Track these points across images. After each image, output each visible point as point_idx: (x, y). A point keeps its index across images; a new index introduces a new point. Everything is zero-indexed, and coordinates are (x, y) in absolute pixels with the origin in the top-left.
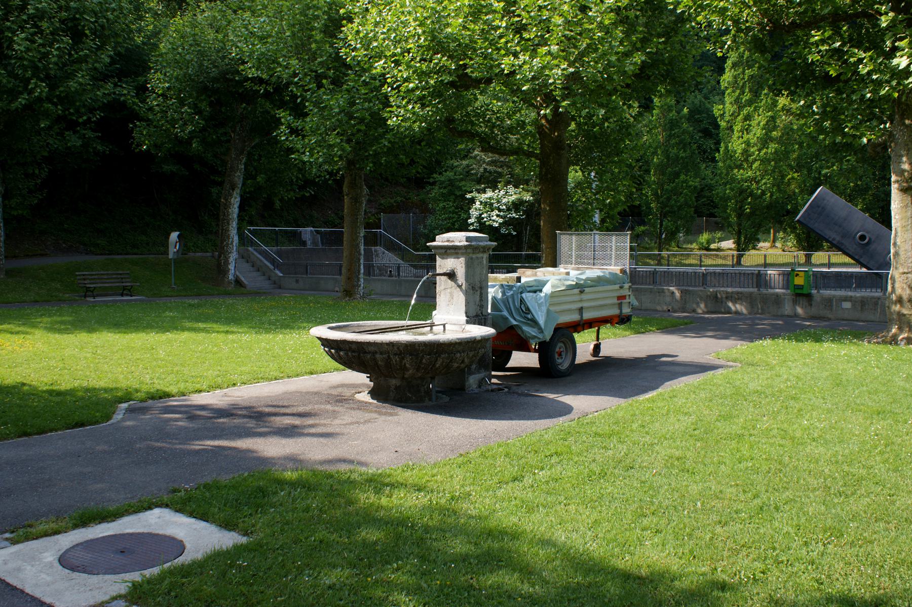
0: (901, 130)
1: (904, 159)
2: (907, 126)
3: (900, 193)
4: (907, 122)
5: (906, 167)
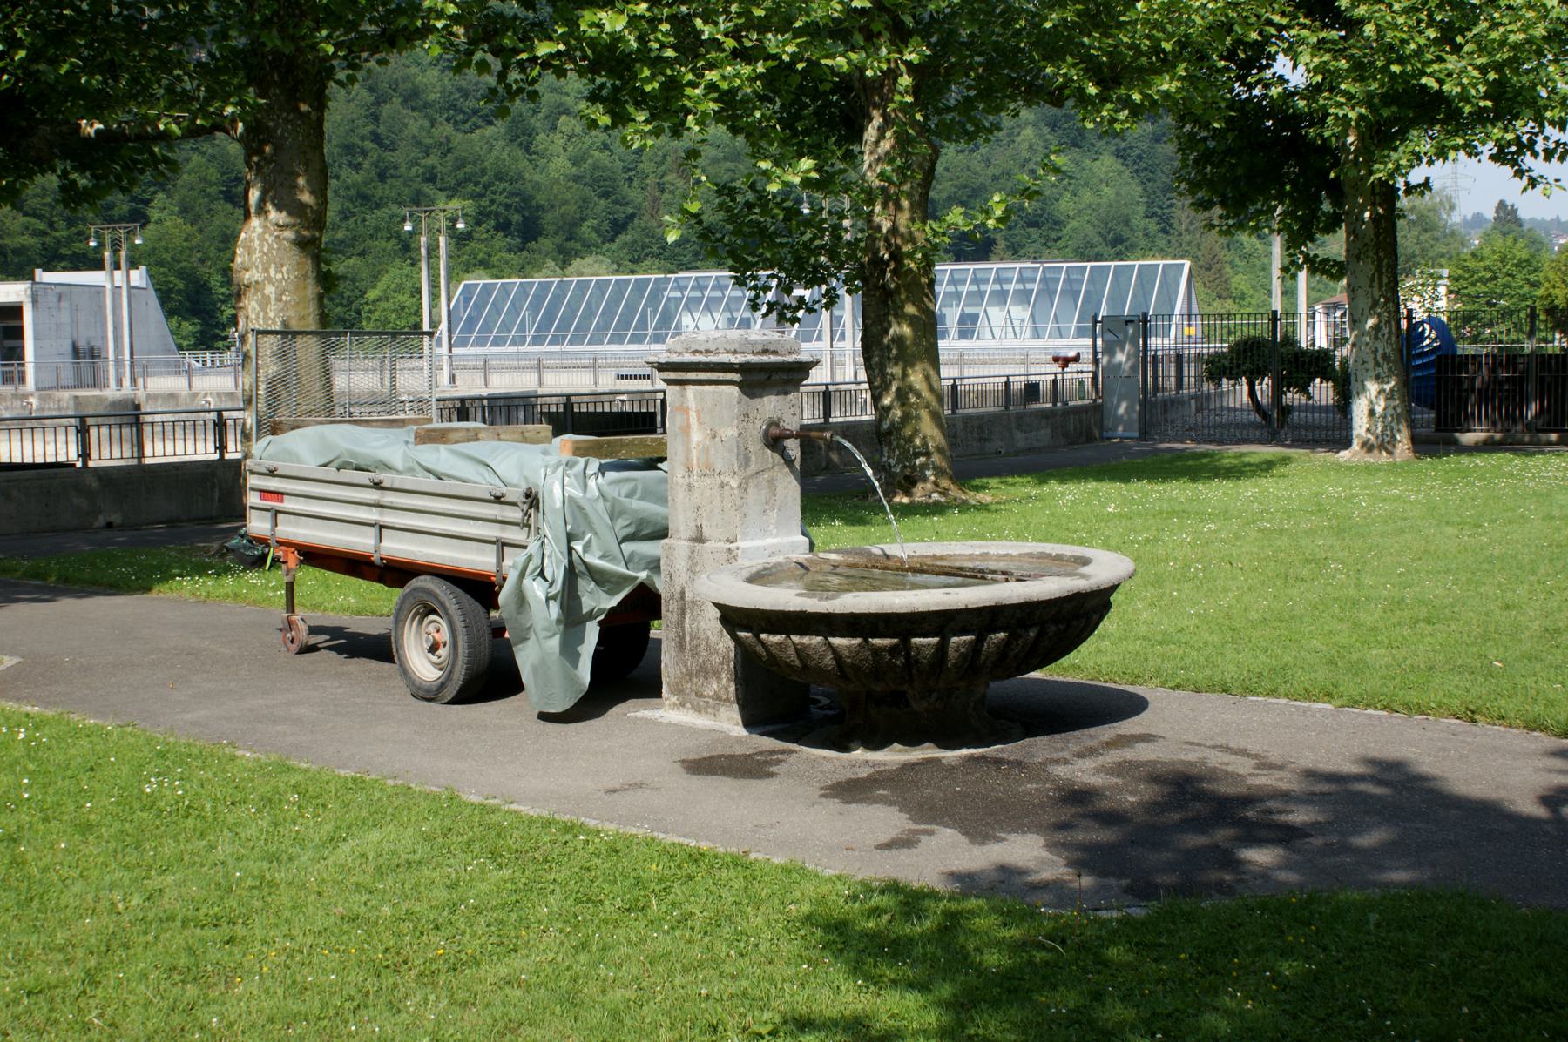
0: (287, 121)
1: (301, 181)
2: (302, 115)
3: (296, 251)
4: (304, 108)
5: (306, 197)
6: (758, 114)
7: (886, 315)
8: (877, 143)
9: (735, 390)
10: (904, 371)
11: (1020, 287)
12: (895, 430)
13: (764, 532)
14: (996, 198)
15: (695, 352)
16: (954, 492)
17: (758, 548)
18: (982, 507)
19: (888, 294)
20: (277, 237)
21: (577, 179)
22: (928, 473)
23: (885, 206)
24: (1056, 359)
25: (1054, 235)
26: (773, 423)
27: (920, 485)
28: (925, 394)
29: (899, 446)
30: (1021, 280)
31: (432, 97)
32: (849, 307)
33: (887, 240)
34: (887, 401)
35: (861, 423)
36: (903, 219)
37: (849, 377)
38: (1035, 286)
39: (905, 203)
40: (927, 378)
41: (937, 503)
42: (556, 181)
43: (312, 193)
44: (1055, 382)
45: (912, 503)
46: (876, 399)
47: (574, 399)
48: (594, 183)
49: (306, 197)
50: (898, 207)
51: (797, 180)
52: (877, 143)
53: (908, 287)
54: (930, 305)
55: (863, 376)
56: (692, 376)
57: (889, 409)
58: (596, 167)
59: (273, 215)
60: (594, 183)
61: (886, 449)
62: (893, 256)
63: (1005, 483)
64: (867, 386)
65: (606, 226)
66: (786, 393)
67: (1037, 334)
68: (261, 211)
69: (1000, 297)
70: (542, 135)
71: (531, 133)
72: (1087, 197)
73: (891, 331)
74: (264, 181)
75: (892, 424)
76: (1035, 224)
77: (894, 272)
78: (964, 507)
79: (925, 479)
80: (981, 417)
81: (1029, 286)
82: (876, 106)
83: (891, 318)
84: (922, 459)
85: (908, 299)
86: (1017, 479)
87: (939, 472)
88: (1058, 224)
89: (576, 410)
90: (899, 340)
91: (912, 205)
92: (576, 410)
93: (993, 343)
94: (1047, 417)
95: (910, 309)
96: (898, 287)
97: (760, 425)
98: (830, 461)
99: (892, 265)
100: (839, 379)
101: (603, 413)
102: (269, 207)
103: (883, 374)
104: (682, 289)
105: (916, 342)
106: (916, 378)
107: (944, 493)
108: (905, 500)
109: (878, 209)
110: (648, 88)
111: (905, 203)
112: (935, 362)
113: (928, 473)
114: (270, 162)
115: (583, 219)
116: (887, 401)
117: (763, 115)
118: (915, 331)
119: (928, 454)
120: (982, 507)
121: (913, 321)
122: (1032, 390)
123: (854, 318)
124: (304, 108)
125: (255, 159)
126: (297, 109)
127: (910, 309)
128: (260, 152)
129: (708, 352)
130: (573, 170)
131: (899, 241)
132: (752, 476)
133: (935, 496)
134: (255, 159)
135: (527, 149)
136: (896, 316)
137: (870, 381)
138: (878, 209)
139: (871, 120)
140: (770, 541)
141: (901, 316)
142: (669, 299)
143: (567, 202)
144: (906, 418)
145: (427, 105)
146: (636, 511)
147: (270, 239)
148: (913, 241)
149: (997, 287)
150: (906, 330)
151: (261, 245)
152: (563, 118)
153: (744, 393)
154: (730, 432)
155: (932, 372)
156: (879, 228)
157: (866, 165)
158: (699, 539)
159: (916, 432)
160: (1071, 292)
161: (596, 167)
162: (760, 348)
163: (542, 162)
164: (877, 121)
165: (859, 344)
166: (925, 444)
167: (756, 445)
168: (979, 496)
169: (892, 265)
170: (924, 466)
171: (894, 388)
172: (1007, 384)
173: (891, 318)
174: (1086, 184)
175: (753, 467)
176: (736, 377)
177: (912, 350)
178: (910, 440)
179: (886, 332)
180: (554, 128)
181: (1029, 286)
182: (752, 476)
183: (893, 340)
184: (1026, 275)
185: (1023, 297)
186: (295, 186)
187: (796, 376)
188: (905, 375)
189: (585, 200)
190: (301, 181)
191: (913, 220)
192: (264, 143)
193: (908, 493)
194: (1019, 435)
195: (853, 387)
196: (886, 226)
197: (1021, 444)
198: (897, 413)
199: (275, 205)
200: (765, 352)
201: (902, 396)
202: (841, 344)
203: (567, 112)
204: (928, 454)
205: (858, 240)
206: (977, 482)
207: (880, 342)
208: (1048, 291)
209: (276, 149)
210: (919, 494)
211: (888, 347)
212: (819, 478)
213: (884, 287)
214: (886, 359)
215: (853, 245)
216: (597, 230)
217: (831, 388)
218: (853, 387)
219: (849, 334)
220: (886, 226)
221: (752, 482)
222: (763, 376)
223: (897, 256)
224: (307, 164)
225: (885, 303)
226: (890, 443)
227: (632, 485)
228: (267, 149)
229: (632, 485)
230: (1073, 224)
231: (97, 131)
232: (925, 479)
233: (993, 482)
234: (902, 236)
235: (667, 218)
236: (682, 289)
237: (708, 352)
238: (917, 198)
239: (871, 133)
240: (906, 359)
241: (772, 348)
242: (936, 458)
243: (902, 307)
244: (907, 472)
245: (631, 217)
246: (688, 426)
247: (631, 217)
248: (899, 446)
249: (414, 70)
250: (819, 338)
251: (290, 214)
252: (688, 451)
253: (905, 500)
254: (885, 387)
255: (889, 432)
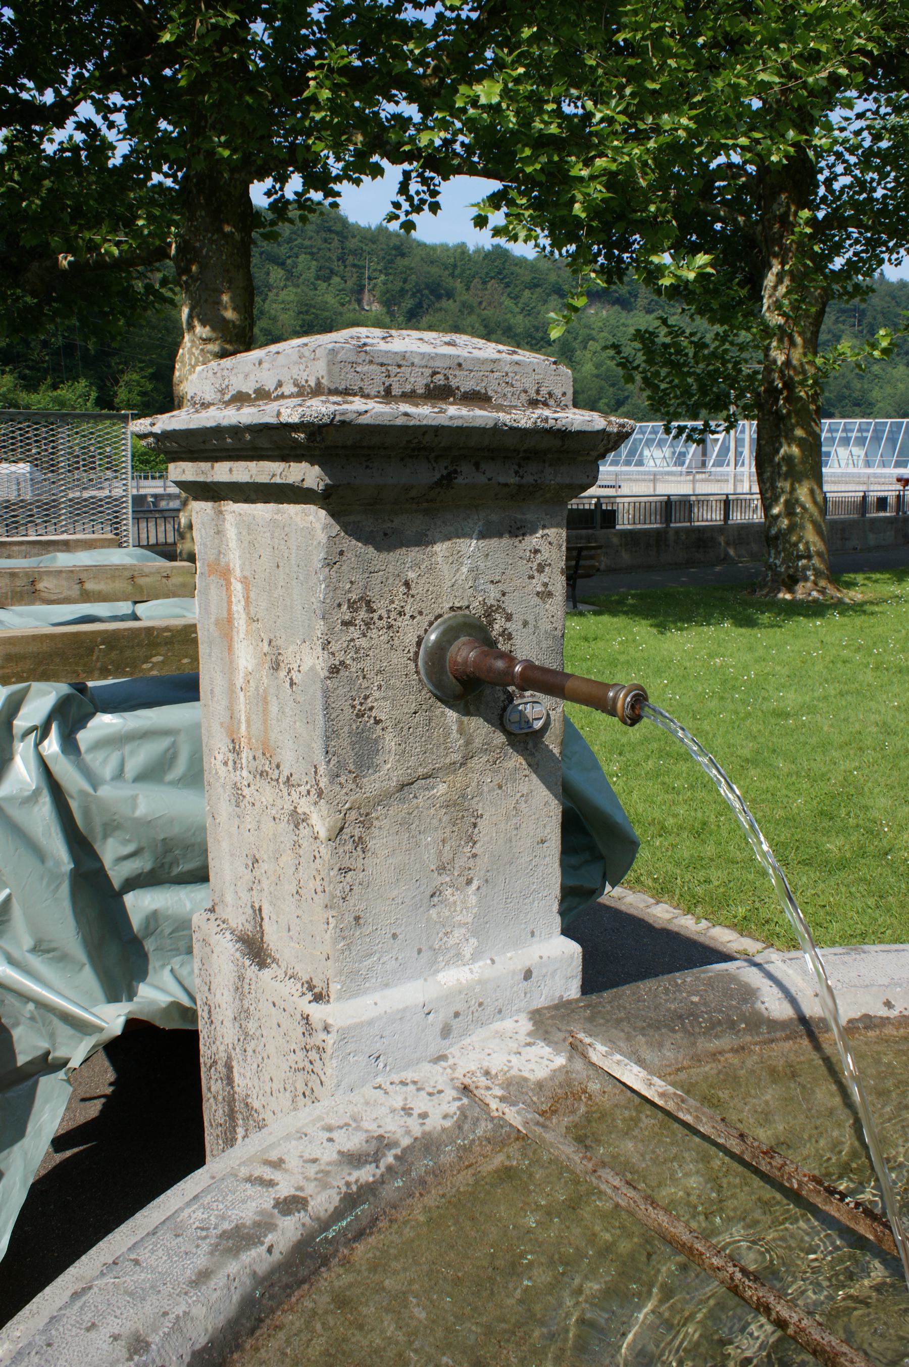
0: (212, 241)
1: (225, 298)
5: (230, 314)
6: (652, 208)
7: (779, 436)
8: (775, 288)
9: (313, 520)
10: (792, 485)
11: (859, 435)
12: (782, 536)
13: (434, 955)
14: (882, 332)
15: (240, 399)
16: (832, 591)
17: (402, 1015)
18: (858, 608)
19: (780, 418)
20: (202, 350)
21: (597, 376)
22: (809, 573)
23: (781, 341)
24: (899, 480)
25: (868, 411)
26: (475, 628)
27: (801, 584)
28: (809, 505)
29: (784, 550)
30: (860, 430)
31: (519, 331)
32: (748, 429)
33: (781, 372)
34: (776, 511)
35: (753, 525)
36: (797, 355)
37: (746, 489)
38: (869, 435)
39: (799, 340)
40: (812, 492)
41: (815, 601)
42: (586, 378)
43: (234, 309)
44: (898, 497)
45: (794, 599)
46: (767, 508)
47: (602, 500)
48: (607, 379)
49: (230, 314)
50: (793, 344)
51: (691, 276)
52: (775, 288)
53: (798, 413)
54: (817, 429)
55: (756, 489)
56: (224, 472)
57: (777, 517)
58: (608, 370)
59: (199, 330)
60: (607, 379)
61: (773, 552)
62: (785, 385)
63: (868, 579)
64: (759, 496)
65: (613, 402)
66: (519, 530)
67: (868, 464)
68: (191, 327)
69: (845, 441)
70: (579, 352)
71: (573, 351)
72: (889, 390)
73: (782, 451)
74: (191, 298)
75: (780, 530)
76: (858, 405)
77: (786, 400)
78: (841, 607)
79: (806, 579)
80: (843, 522)
81: (865, 434)
82: (776, 256)
83: (783, 440)
84: (804, 561)
85: (798, 424)
86: (878, 576)
87: (818, 573)
88: (871, 405)
89: (604, 507)
90: (789, 459)
91: (804, 340)
92: (604, 507)
93: (839, 470)
94: (892, 523)
95: (799, 432)
96: (789, 412)
97: (416, 631)
98: (727, 555)
99: (785, 394)
100: (739, 491)
101: (584, 510)
102: (196, 323)
103: (774, 487)
104: (644, 433)
105: (804, 461)
106: (803, 493)
107: (822, 591)
108: (788, 597)
109: (774, 344)
110: (529, 170)
111: (799, 340)
112: (818, 478)
113: (809, 573)
114: (196, 281)
115: (600, 399)
116: (776, 511)
117: (658, 209)
118: (802, 450)
119: (809, 557)
120: (858, 608)
121: (801, 443)
122: (882, 503)
123: (751, 452)
124: (227, 229)
125: (184, 278)
126: (221, 230)
127: (799, 432)
128: (187, 271)
129: (262, 395)
130: (595, 372)
131: (791, 373)
132: (384, 798)
133: (815, 594)
134: (184, 278)
135: (570, 359)
136: (786, 437)
137: (761, 493)
138: (774, 344)
139: (771, 268)
140: (453, 976)
141: (791, 439)
142: (635, 440)
143: (591, 389)
144: (792, 528)
145: (516, 335)
146: (147, 823)
147: (197, 352)
148: (804, 372)
149: (844, 435)
150: (795, 450)
151: (190, 359)
152: (591, 342)
153: (353, 530)
154: (310, 661)
155: (815, 487)
156: (775, 362)
157: (765, 308)
158: (255, 950)
159: (801, 538)
160: (892, 440)
161: (608, 370)
162: (419, 383)
163: (578, 367)
164: (776, 268)
165: (754, 470)
166: (807, 548)
167: (397, 692)
168: (852, 593)
169: (785, 394)
170: (806, 568)
171: (782, 500)
172: (864, 497)
173: (783, 440)
174: (889, 382)
175: (389, 769)
176: (307, 474)
177: (800, 468)
178: (796, 545)
179: (778, 451)
180: (585, 348)
181: (865, 434)
182: (384, 798)
183: (783, 458)
184: (864, 427)
185: (861, 441)
186: (219, 302)
187: (552, 477)
188: (793, 490)
189: (602, 388)
190: (225, 298)
191: (805, 355)
192: (190, 262)
193: (791, 590)
194: (871, 536)
195: (748, 497)
196: (781, 358)
197: (872, 543)
198: (785, 523)
199: (200, 320)
200: (439, 393)
201: (790, 507)
202: (742, 469)
203: (593, 339)
204: (809, 557)
205: (756, 373)
206: (848, 577)
207: (772, 460)
208: (877, 438)
209: (202, 267)
210: (801, 591)
211: (779, 463)
212: (718, 569)
213: (778, 412)
214: (777, 473)
215: (751, 377)
216: (607, 405)
217: (731, 497)
218: (748, 497)
219: (747, 462)
220: (781, 358)
221: (385, 822)
222: (424, 475)
223: (789, 385)
224: (230, 281)
225: (777, 426)
226: (776, 547)
227: (165, 743)
228: (194, 268)
229: (165, 743)
230: (880, 405)
231: (70, 263)
232: (806, 579)
233: (860, 578)
234: (794, 368)
235: (552, 315)
236: (644, 433)
237: (262, 395)
238: (809, 335)
239: (770, 279)
240: (795, 477)
241: (465, 383)
242: (816, 561)
243: (792, 430)
244: (791, 571)
245: (627, 398)
246: (230, 620)
247: (627, 398)
248: (784, 550)
249: (509, 315)
250: (728, 465)
251: (213, 329)
252: (231, 691)
253: (788, 597)
254: (776, 499)
255: (777, 537)
